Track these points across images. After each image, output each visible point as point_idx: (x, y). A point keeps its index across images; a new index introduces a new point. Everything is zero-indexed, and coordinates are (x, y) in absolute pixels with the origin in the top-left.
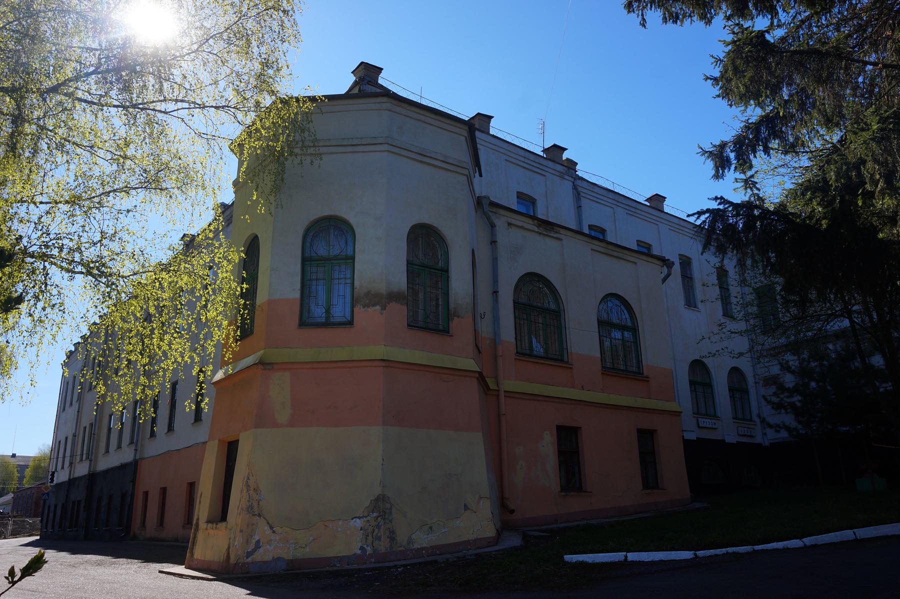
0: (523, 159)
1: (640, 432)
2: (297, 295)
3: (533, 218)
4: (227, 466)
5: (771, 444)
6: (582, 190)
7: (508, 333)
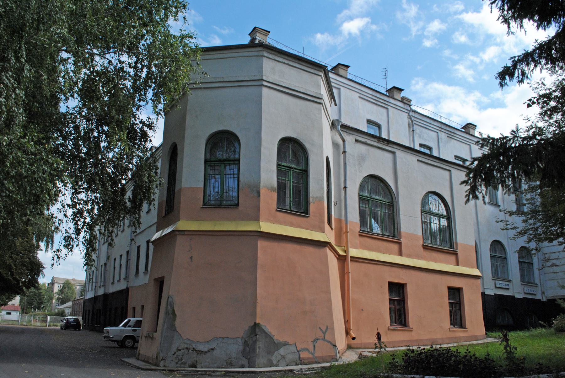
2: (202, 185)
6: (416, 120)
7: (354, 216)
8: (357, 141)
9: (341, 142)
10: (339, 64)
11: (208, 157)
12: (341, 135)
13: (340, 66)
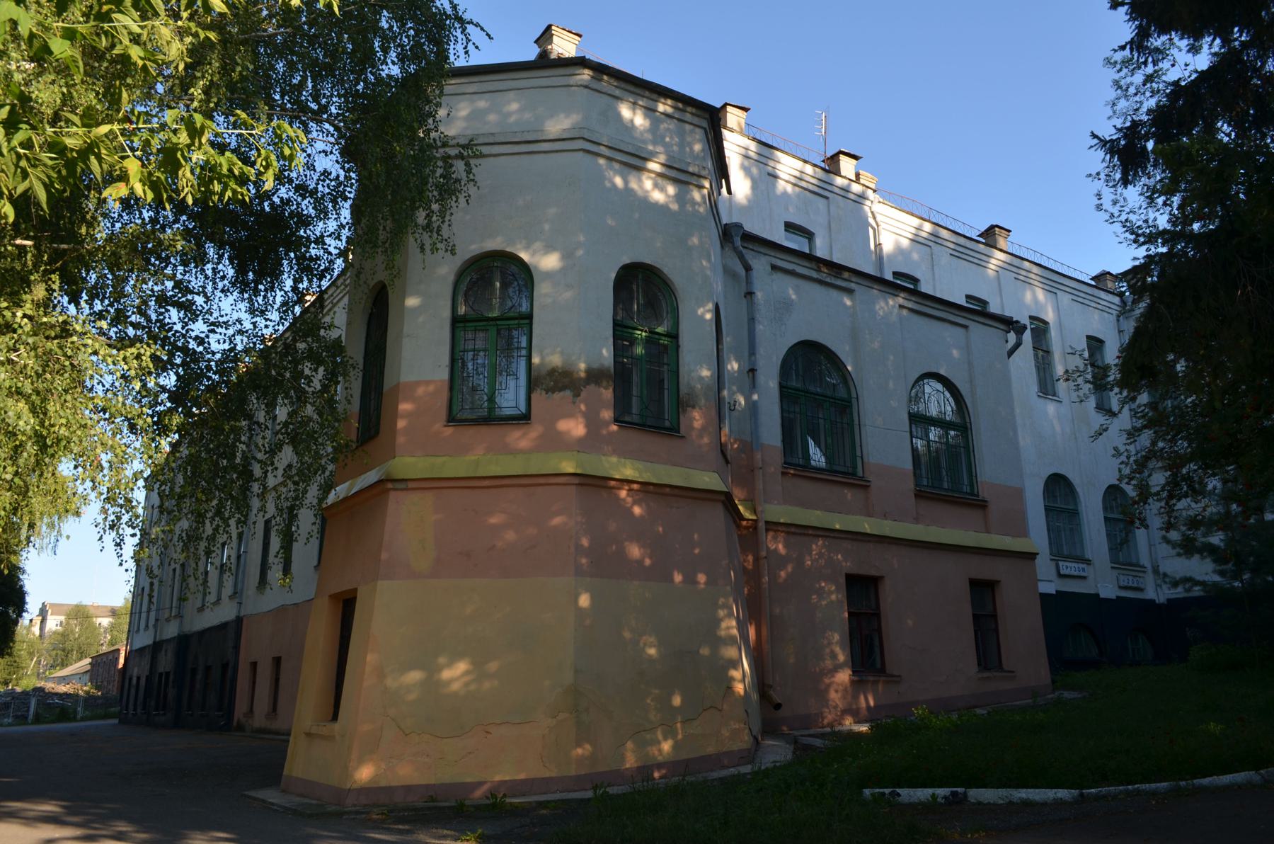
1: (975, 584)
2: (444, 375)
5: (1168, 600)
7: (771, 433)
8: (774, 268)
9: (743, 272)
11: (462, 310)
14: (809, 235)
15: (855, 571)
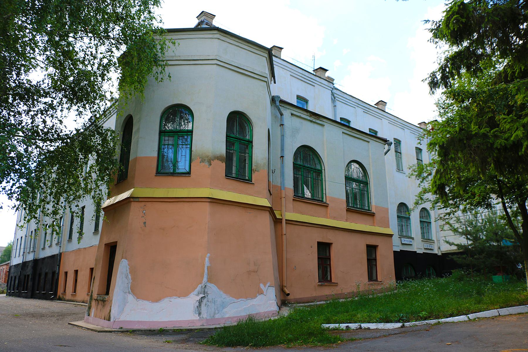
0: (301, 75)
3: (307, 111)
4: (110, 261)
6: (336, 95)
7: (289, 184)
8: (292, 114)
10: (274, 46)
12: (279, 110)
13: (275, 48)
14: (306, 101)
15: (321, 240)
